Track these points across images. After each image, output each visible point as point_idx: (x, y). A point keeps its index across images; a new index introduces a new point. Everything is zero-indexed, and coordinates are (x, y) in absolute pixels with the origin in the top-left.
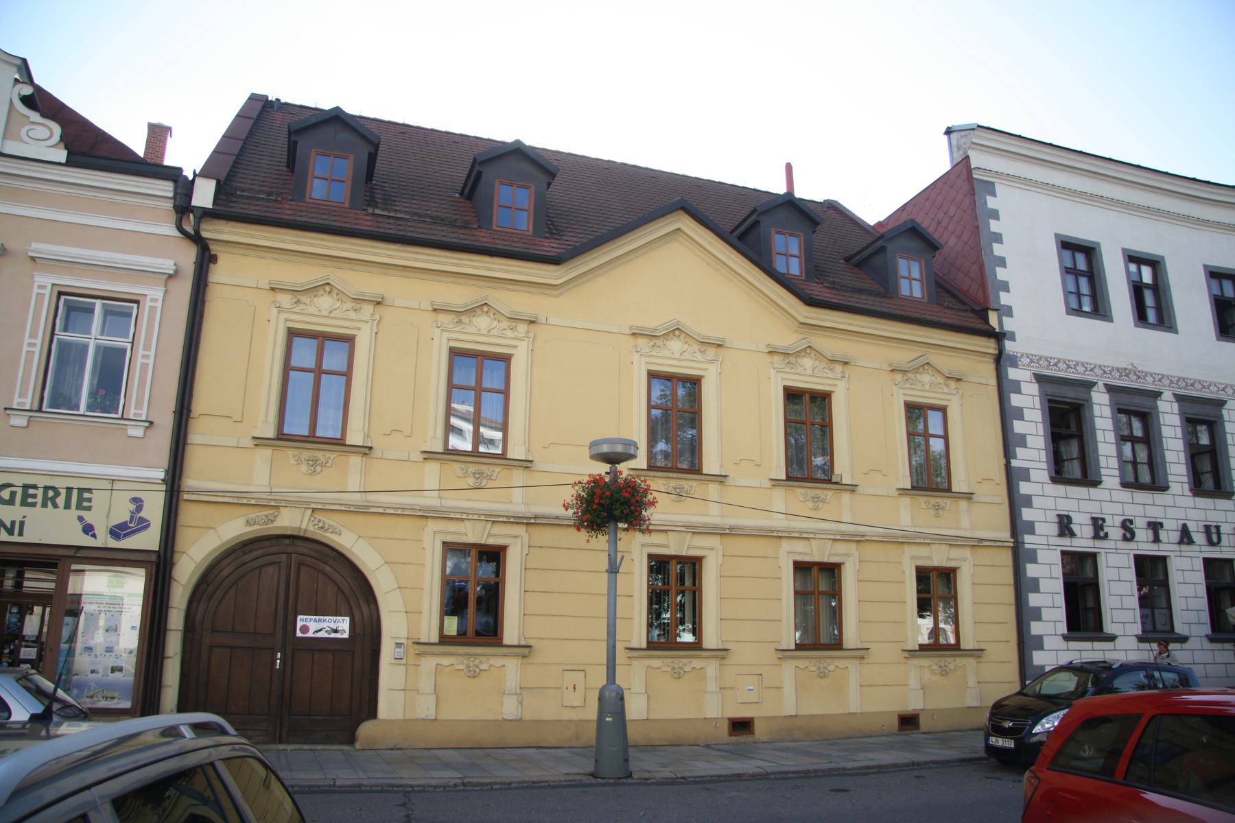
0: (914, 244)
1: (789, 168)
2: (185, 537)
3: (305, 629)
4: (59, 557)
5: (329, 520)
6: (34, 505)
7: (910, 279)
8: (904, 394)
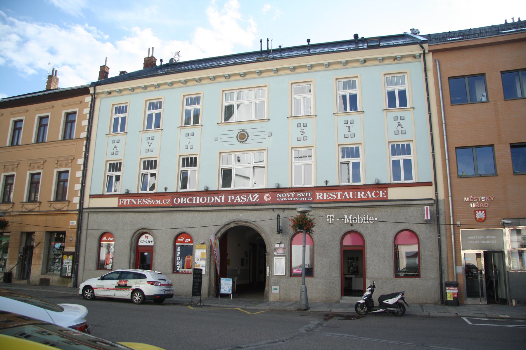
1: (106, 58)
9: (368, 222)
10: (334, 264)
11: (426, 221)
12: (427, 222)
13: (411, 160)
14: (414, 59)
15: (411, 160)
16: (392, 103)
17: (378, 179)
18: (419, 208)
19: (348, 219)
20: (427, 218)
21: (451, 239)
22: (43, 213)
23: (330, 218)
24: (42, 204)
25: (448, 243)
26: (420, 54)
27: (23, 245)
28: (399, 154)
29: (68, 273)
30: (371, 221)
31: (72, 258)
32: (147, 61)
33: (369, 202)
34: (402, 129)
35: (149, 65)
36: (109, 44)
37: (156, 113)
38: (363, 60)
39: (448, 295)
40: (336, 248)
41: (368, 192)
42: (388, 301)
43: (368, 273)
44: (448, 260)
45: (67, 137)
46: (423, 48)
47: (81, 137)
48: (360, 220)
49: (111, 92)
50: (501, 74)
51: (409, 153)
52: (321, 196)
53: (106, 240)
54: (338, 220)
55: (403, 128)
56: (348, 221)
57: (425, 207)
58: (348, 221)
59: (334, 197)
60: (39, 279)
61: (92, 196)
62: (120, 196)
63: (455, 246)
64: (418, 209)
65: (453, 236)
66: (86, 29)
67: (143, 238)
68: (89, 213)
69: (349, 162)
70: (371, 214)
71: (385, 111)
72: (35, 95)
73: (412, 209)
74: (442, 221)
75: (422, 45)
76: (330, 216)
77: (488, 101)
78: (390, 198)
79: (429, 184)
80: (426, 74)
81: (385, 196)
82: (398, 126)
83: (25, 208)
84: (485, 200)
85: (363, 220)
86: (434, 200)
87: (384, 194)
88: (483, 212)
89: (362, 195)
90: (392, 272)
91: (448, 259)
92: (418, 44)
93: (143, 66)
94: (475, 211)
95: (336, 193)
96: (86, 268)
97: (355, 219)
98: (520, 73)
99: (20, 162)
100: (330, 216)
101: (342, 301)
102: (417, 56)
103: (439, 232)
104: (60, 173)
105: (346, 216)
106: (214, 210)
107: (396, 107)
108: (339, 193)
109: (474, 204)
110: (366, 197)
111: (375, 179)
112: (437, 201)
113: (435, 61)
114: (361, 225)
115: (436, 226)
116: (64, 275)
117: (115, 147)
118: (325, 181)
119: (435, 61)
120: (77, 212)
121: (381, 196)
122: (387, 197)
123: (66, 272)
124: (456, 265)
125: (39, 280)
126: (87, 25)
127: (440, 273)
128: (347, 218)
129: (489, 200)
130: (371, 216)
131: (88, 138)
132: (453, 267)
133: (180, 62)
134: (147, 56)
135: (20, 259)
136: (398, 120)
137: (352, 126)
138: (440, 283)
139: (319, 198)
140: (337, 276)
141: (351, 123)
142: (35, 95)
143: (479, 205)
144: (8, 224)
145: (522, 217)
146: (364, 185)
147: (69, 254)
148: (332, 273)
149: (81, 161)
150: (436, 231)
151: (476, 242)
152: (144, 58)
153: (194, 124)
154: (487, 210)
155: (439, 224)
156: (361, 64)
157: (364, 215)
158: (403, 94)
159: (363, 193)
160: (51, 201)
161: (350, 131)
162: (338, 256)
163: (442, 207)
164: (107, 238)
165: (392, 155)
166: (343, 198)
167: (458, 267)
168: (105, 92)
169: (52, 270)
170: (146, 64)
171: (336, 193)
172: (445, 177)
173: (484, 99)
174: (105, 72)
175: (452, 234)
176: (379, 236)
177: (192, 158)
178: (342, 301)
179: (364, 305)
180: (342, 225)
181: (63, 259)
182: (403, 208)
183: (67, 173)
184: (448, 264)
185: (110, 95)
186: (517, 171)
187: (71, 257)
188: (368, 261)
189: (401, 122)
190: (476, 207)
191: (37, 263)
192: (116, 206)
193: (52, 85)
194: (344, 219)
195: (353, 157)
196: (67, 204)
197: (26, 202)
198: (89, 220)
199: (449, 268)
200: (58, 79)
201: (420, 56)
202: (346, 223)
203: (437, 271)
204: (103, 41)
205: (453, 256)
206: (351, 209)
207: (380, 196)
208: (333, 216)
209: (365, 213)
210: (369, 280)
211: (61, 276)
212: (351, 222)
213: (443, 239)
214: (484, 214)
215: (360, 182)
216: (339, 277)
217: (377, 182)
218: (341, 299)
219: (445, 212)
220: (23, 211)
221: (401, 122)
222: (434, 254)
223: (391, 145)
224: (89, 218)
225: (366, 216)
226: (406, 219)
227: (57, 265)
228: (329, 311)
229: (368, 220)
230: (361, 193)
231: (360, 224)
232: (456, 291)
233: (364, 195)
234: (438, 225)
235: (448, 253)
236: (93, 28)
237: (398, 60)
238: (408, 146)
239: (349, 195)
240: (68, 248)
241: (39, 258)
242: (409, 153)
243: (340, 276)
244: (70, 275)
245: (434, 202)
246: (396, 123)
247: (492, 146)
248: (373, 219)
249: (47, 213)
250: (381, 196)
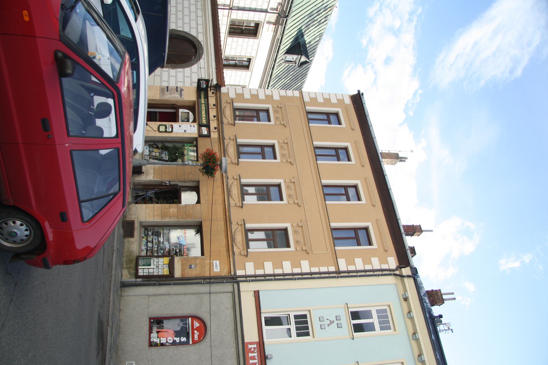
1: (432, 231)
22: (227, 214)
24: (233, 126)
27: (180, 184)
29: (143, 269)
31: (165, 274)
32: (438, 295)
34: (326, 326)
35: (432, 299)
36: (404, 116)
37: (373, 322)
45: (310, 116)
47: (338, 259)
49: (408, 300)
53: (195, 328)
55: (328, 326)
60: (133, 219)
61: (257, 294)
62: (261, 344)
66: (416, 91)
68: (232, 292)
72: (407, 250)
82: (330, 321)
83: (226, 106)
93: (430, 289)
96: (151, 299)
99: (295, 165)
104: (267, 111)
106: (236, 312)
111: (272, 355)
116: (140, 262)
117: (332, 322)
120: (232, 273)
123: (144, 265)
125: (131, 219)
126: (420, 91)
131: (338, 274)
133: (439, 333)
134: (442, 292)
135: (162, 182)
142: (403, 233)
144: (210, 175)
147: (171, 266)
149: (305, 267)
152: (440, 290)
153: (354, 325)
160: (245, 225)
164: (197, 329)
168: (406, 293)
169: (146, 232)
170: (433, 294)
174: (414, 233)
177: (307, 328)
181: (163, 257)
183: (273, 157)
185: (402, 299)
187: (166, 272)
189: (335, 325)
191: (156, 213)
192: (246, 341)
193: (387, 160)
195: (297, 329)
196: (230, 122)
197: (236, 142)
198: (222, 295)
200: (395, 164)
204: (406, 111)
211: (138, 258)
217: (268, 357)
220: (229, 180)
221: (335, 325)
224: (225, 294)
227: (154, 239)
236: (418, 98)
240: (180, 262)
241: (163, 215)
244: (141, 273)
249: (228, 221)
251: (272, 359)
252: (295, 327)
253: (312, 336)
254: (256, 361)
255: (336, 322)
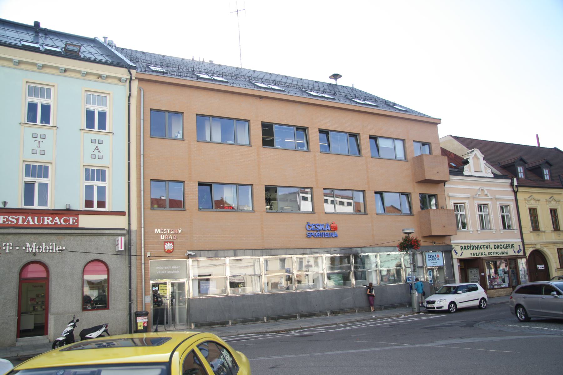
0: (521, 162)
1: (537, 136)
2: (526, 251)
3: (539, 268)
4: (515, 258)
5: (542, 246)
6: (508, 248)
7: (521, 173)
8: (550, 207)
9: (54, 251)
10: (9, 301)
11: (119, 251)
12: (119, 253)
13: (105, 187)
14: (119, 82)
15: (105, 187)
16: (90, 124)
17: (69, 205)
18: (111, 238)
19: (31, 248)
20: (121, 248)
21: (142, 269)
23: (8, 247)
25: (138, 273)
26: (127, 79)
28: (93, 179)
30: (58, 250)
33: (57, 229)
34: (99, 153)
38: (64, 69)
39: (139, 325)
40: (13, 281)
41: (57, 218)
42: (91, 335)
43: (52, 308)
44: (137, 290)
46: (130, 74)
48: (46, 249)
49: (67, 69)
50: (151, 111)
51: (104, 180)
52: (50, 221)
54: (17, 248)
55: (100, 152)
56: (30, 250)
57: (120, 237)
58: (30, 250)
59: (13, 222)
63: (145, 276)
64: (110, 238)
65: (143, 266)
67: (31, 267)
69: (35, 182)
70: (59, 243)
71: (22, 125)
73: (104, 238)
74: (133, 252)
75: (130, 70)
76: (8, 244)
77: (183, 139)
78: (80, 226)
79: (122, 213)
80: (129, 101)
81: (76, 224)
82: (95, 149)
84: (174, 233)
85: (49, 250)
86: (126, 230)
87: (74, 221)
88: (171, 244)
89: (49, 221)
90: (80, 306)
91: (137, 288)
92: (126, 68)
94: (165, 242)
95: (17, 218)
97: (39, 249)
98: (211, 118)
100: (8, 244)
101: (18, 344)
102: (123, 80)
103: (130, 262)
105: (28, 244)
107: (105, 129)
108: (21, 218)
109: (164, 236)
110: (53, 224)
112: (129, 231)
113: (140, 90)
114: (47, 255)
115: (127, 257)
118: (2, 202)
119: (140, 90)
121: (71, 223)
122: (78, 224)
124: (145, 295)
127: (129, 303)
128: (29, 247)
129: (177, 233)
130: (59, 245)
132: (142, 297)
136: (95, 143)
137: (42, 141)
138: (129, 313)
139: (47, 222)
140: (13, 315)
141: (41, 138)
143: (168, 237)
145: (203, 250)
146: (53, 210)
148: (6, 311)
150: (127, 262)
151: (163, 272)
154: (175, 241)
155: (130, 255)
156: (60, 72)
157: (51, 244)
158: (102, 115)
159: (51, 219)
161: (39, 147)
162: (15, 290)
163: (133, 237)
165: (86, 180)
166: (26, 223)
167: (146, 296)
171: (17, 217)
172: (139, 208)
173: (180, 136)
175: (143, 264)
176: (66, 266)
177: (40, 167)
178: (18, 344)
179: (64, 342)
180: (23, 254)
182: (95, 237)
184: (137, 295)
186: (201, 207)
188: (52, 294)
189: (99, 146)
190: (166, 238)
194: (26, 248)
195: (40, 176)
199: (138, 298)
201: (126, 81)
202: (27, 252)
203: (127, 301)
205: (142, 286)
206: (35, 236)
207: (70, 223)
208: (11, 244)
209: (52, 241)
210: (53, 316)
212: (34, 251)
213: (133, 269)
214: (172, 246)
215: (46, 205)
216: (15, 316)
218: (17, 342)
219: (137, 243)
221: (99, 146)
222: (124, 284)
223: (26, 165)
225: (52, 245)
226: (97, 249)
228: (16, 355)
229: (54, 249)
230: (48, 219)
231: (45, 253)
232: (146, 320)
233: (52, 221)
234: (130, 254)
235: (137, 283)
237: (102, 79)
238: (104, 172)
239: (33, 220)
242: (104, 180)
243: (17, 315)
245: (127, 233)
246: (93, 146)
247: (183, 182)
248: (61, 248)
250: (71, 223)
251: (70, 205)
252: (102, 182)
253: (50, 164)
254: (21, 218)
255: (97, 144)
